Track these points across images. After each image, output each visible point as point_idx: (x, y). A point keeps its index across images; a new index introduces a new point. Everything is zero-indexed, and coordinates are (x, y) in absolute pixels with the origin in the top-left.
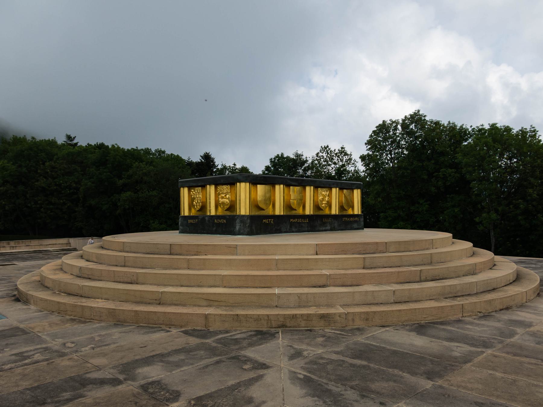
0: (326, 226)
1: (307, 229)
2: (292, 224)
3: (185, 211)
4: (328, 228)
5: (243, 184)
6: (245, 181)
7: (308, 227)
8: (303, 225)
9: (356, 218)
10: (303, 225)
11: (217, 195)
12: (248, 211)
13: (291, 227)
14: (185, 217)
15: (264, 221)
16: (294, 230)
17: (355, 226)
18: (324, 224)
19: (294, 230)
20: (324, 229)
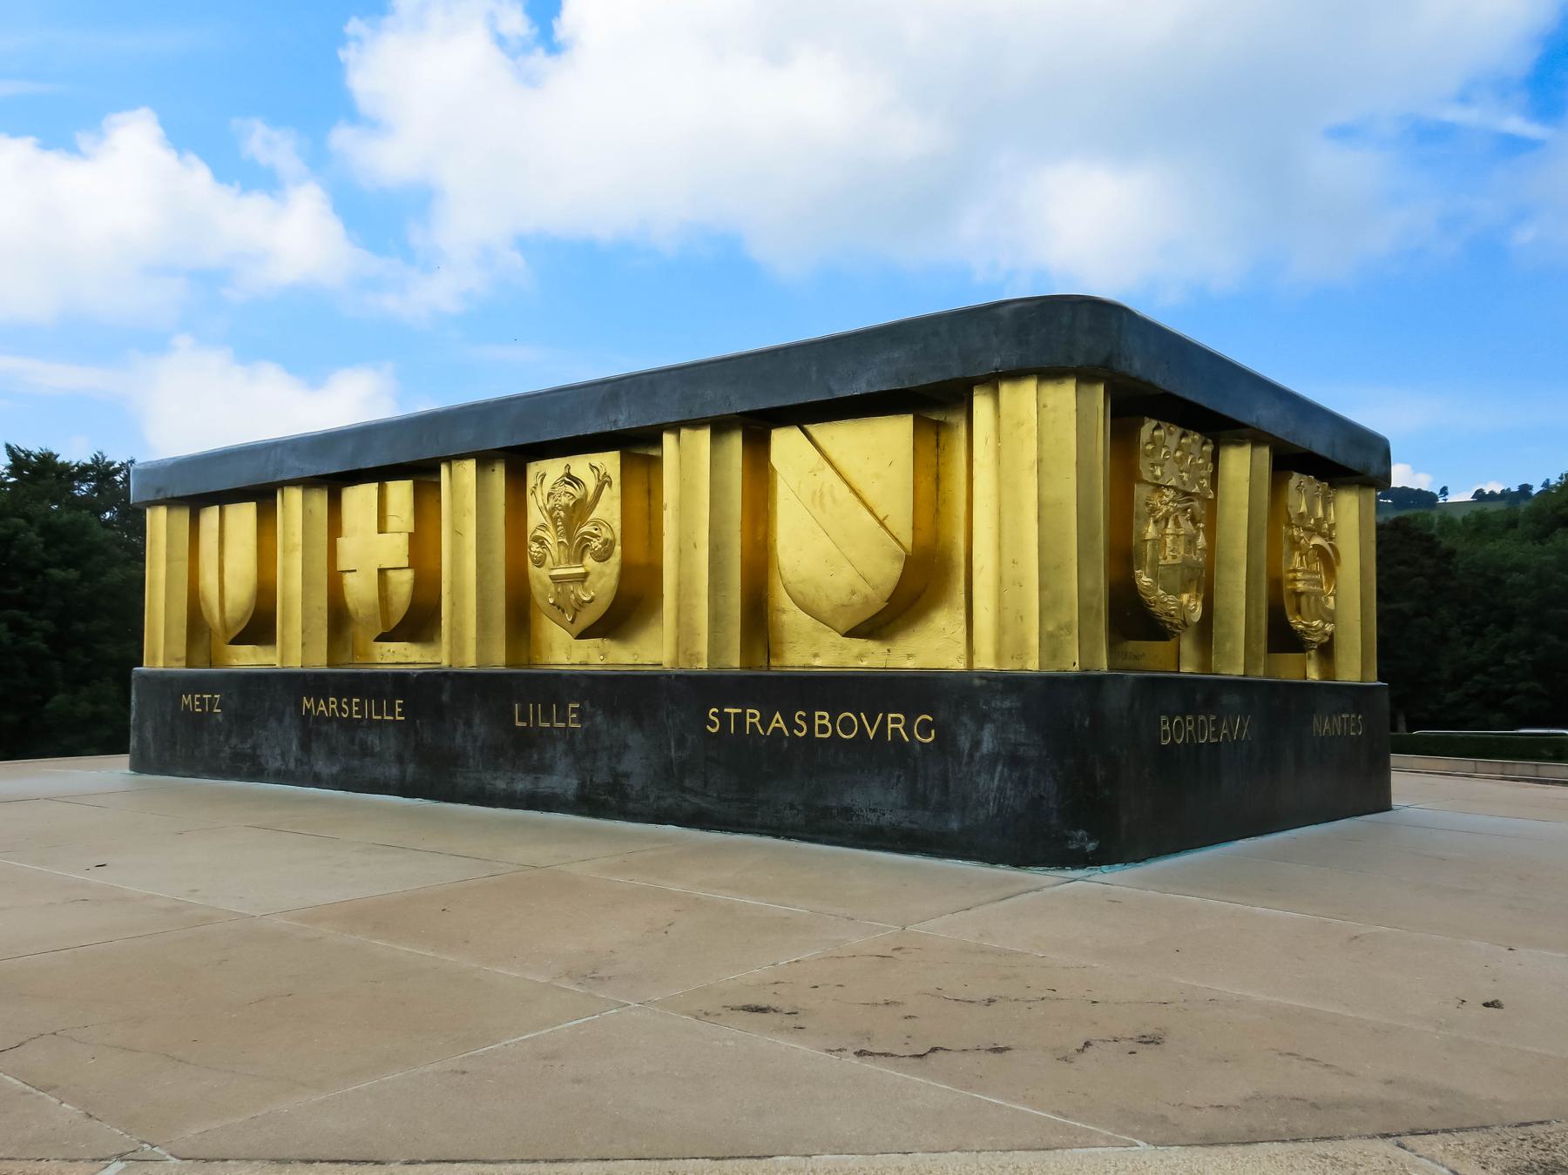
0: (545, 769)
1: (394, 771)
2: (310, 730)
3: (162, 647)
4: (563, 781)
5: (1022, 397)
6: (1048, 374)
7: (400, 759)
8: (373, 740)
9: (895, 722)
10: (373, 740)
11: (1041, 407)
12: (703, 646)
13: (305, 747)
14: (166, 684)
15: (186, 700)
16: (321, 766)
17: (877, 798)
18: (522, 748)
19: (321, 766)
20: (522, 785)
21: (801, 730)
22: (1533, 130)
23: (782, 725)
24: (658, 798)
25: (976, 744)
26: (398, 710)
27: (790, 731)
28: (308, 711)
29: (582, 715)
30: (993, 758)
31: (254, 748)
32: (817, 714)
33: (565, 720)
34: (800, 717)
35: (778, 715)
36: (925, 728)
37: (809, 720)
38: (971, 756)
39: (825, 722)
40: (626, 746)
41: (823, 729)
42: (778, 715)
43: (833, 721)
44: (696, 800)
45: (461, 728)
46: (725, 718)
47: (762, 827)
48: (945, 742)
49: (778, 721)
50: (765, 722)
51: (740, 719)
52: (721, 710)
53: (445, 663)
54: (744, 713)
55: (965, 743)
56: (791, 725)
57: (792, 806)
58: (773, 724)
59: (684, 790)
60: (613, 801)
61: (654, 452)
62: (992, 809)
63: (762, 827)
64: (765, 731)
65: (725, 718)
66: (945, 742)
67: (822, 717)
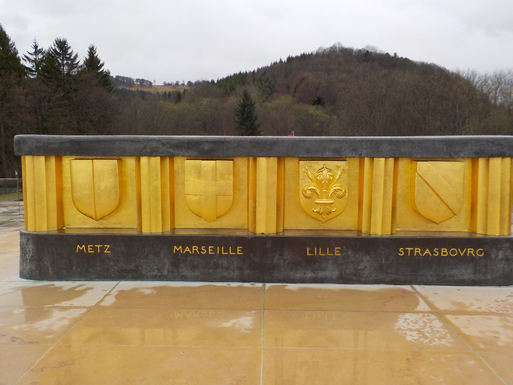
7: (240, 269)
9: (470, 251)
20: (299, 275)
21: (204, 251)
22: (22, 59)
23: (429, 252)
24: (376, 276)
25: (497, 256)
26: (238, 250)
27: (200, 252)
28: (178, 252)
29: (341, 251)
30: (502, 259)
31: (137, 267)
32: (442, 249)
33: (334, 253)
34: (436, 250)
35: (187, 247)
36: (480, 252)
37: (440, 251)
38: (495, 259)
39: (446, 251)
40: (362, 261)
41: (445, 253)
42: (187, 247)
43: (448, 251)
44: (393, 276)
45: (277, 256)
46: (406, 252)
47: (419, 282)
48: (487, 256)
49: (427, 252)
50: (422, 252)
51: (412, 252)
52: (94, 245)
53: (46, 230)
54: (414, 250)
55: (493, 256)
56: (432, 252)
57: (432, 276)
58: (426, 252)
59: (388, 273)
60: (354, 278)
61: (68, 153)
62: (501, 272)
63: (445, 282)
64: (422, 254)
65: (406, 252)
66: (487, 256)
67: (444, 250)
